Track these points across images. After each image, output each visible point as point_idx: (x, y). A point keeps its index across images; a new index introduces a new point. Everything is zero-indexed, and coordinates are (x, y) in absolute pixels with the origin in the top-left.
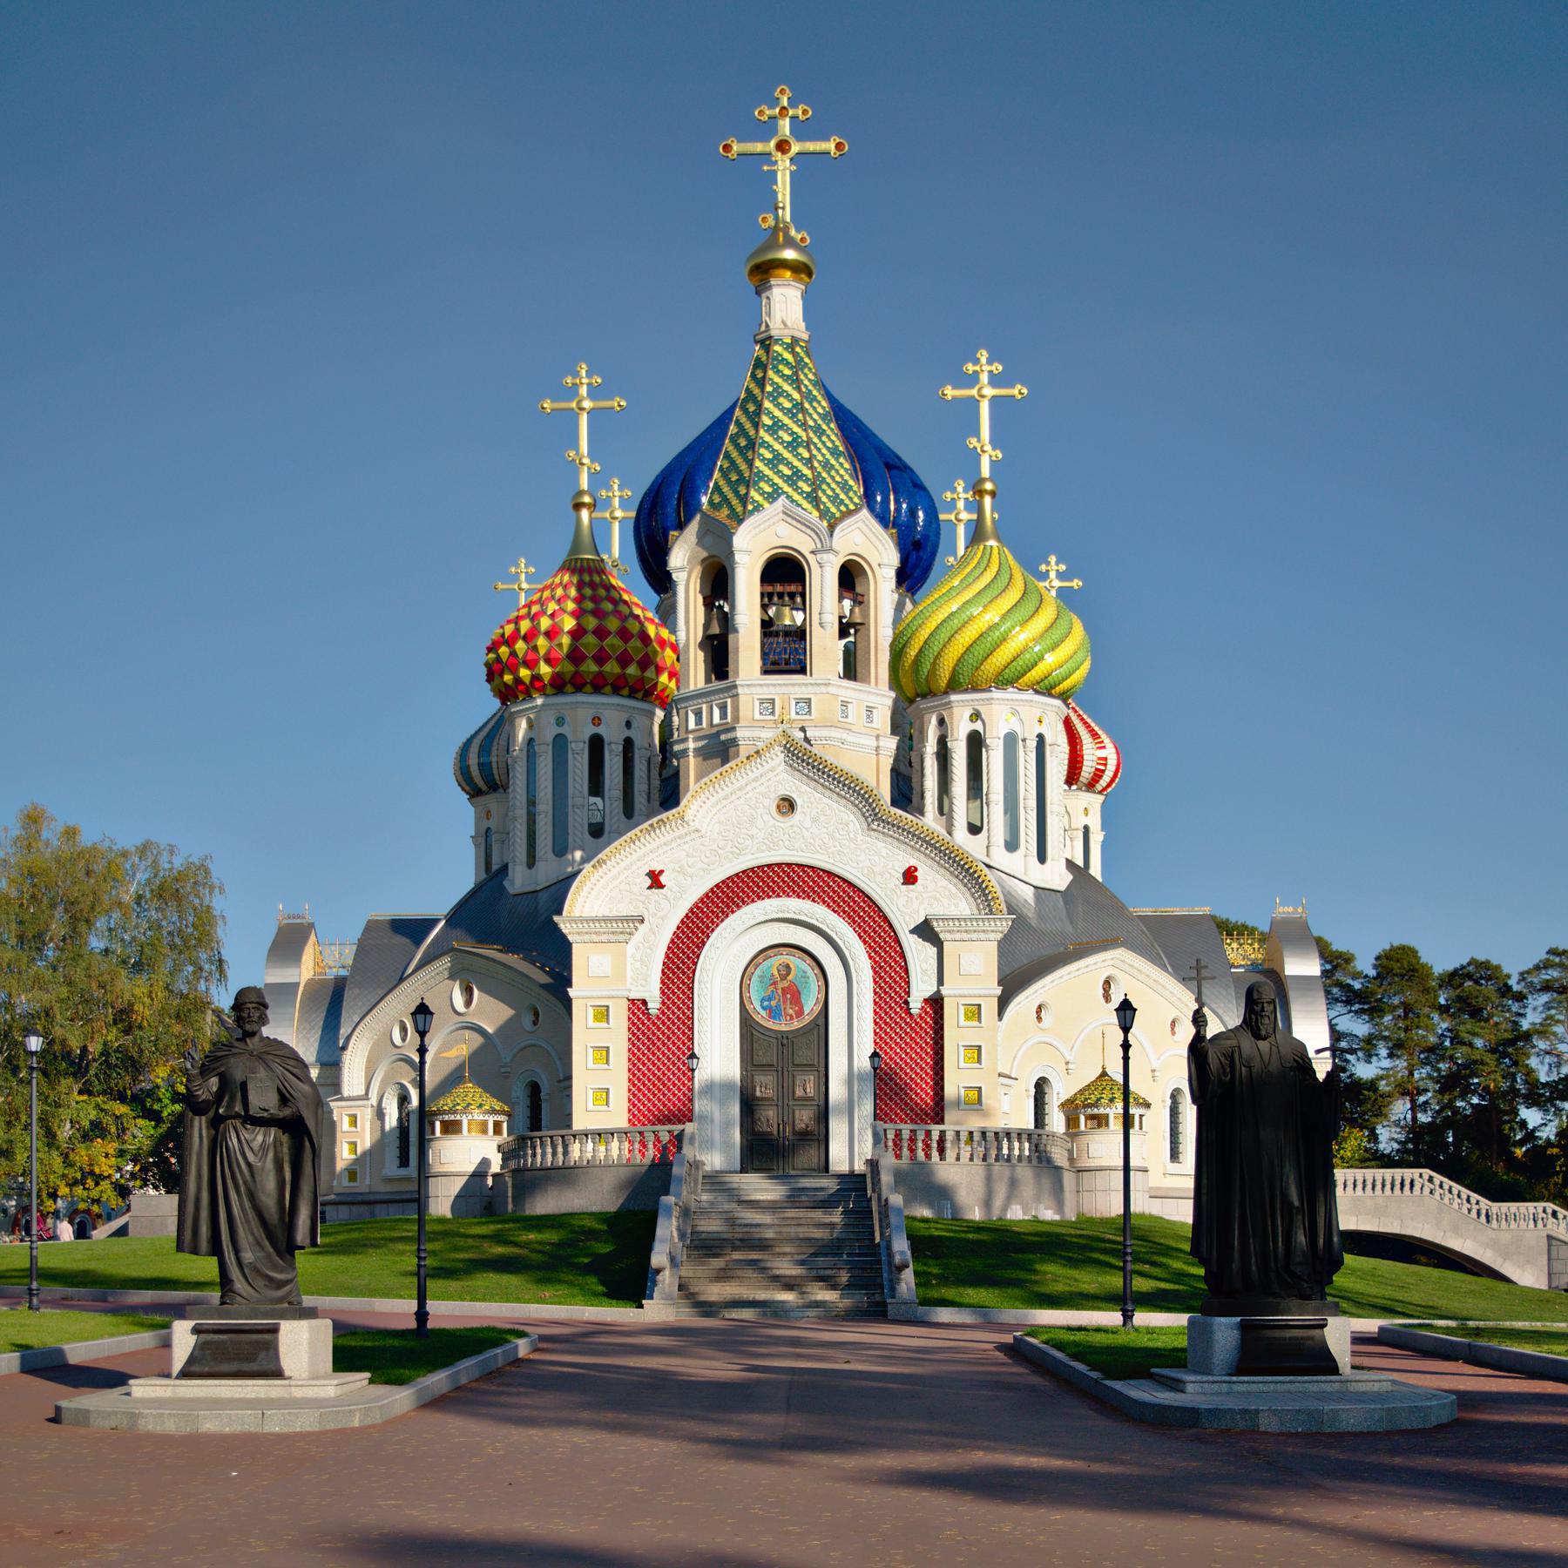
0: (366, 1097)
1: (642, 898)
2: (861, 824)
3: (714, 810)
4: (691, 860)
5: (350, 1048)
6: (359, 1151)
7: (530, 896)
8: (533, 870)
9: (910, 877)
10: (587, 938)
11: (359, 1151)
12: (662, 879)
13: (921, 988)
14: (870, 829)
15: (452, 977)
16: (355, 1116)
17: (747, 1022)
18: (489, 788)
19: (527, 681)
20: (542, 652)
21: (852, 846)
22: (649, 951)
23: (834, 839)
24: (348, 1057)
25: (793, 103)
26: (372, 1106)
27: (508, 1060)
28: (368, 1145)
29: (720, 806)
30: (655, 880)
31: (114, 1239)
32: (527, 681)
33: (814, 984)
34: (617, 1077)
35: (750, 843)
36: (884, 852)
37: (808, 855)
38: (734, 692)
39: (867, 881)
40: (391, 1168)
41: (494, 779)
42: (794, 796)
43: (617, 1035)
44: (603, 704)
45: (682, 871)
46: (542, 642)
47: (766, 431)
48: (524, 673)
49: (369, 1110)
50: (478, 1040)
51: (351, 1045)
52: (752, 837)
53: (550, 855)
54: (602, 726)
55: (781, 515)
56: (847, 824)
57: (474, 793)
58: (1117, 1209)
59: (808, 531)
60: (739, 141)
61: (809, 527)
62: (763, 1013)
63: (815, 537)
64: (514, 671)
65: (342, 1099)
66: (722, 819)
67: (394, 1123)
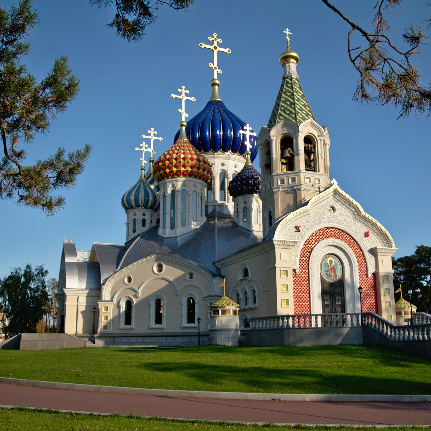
0: (112, 300)
1: (294, 235)
2: (353, 217)
3: (314, 208)
4: (307, 224)
5: (106, 284)
6: (109, 319)
7: (173, 238)
8: (174, 230)
9: (367, 235)
10: (280, 247)
11: (109, 319)
12: (295, 230)
13: (371, 270)
14: (356, 218)
15: (156, 260)
16: (107, 307)
17: (322, 278)
18: (136, 206)
19: (175, 172)
20: (174, 164)
21: (351, 223)
22: (296, 253)
23: (346, 221)
24: (105, 287)
25: (218, 38)
26: (114, 304)
27: (179, 290)
28: (112, 318)
29: (315, 207)
30: (298, 229)
31: (3, 351)
32: (175, 172)
33: (339, 268)
34: (290, 296)
35: (323, 220)
36: (359, 226)
37: (339, 225)
38: (299, 174)
39: (355, 235)
40: (122, 325)
41: (139, 204)
42: (335, 206)
43: (290, 281)
44: (197, 182)
45: (305, 227)
46: (174, 161)
47: (283, 102)
48: (168, 171)
49: (112, 305)
50: (166, 283)
51: (107, 283)
52: (324, 218)
53: (180, 226)
54: (196, 188)
55: (310, 124)
56: (349, 217)
57: (126, 209)
58: (75, 333)
59: (317, 129)
60: (204, 44)
61: (317, 128)
62: (326, 276)
63: (319, 132)
64: (164, 169)
65: (102, 301)
66: (315, 211)
67: (124, 309)
